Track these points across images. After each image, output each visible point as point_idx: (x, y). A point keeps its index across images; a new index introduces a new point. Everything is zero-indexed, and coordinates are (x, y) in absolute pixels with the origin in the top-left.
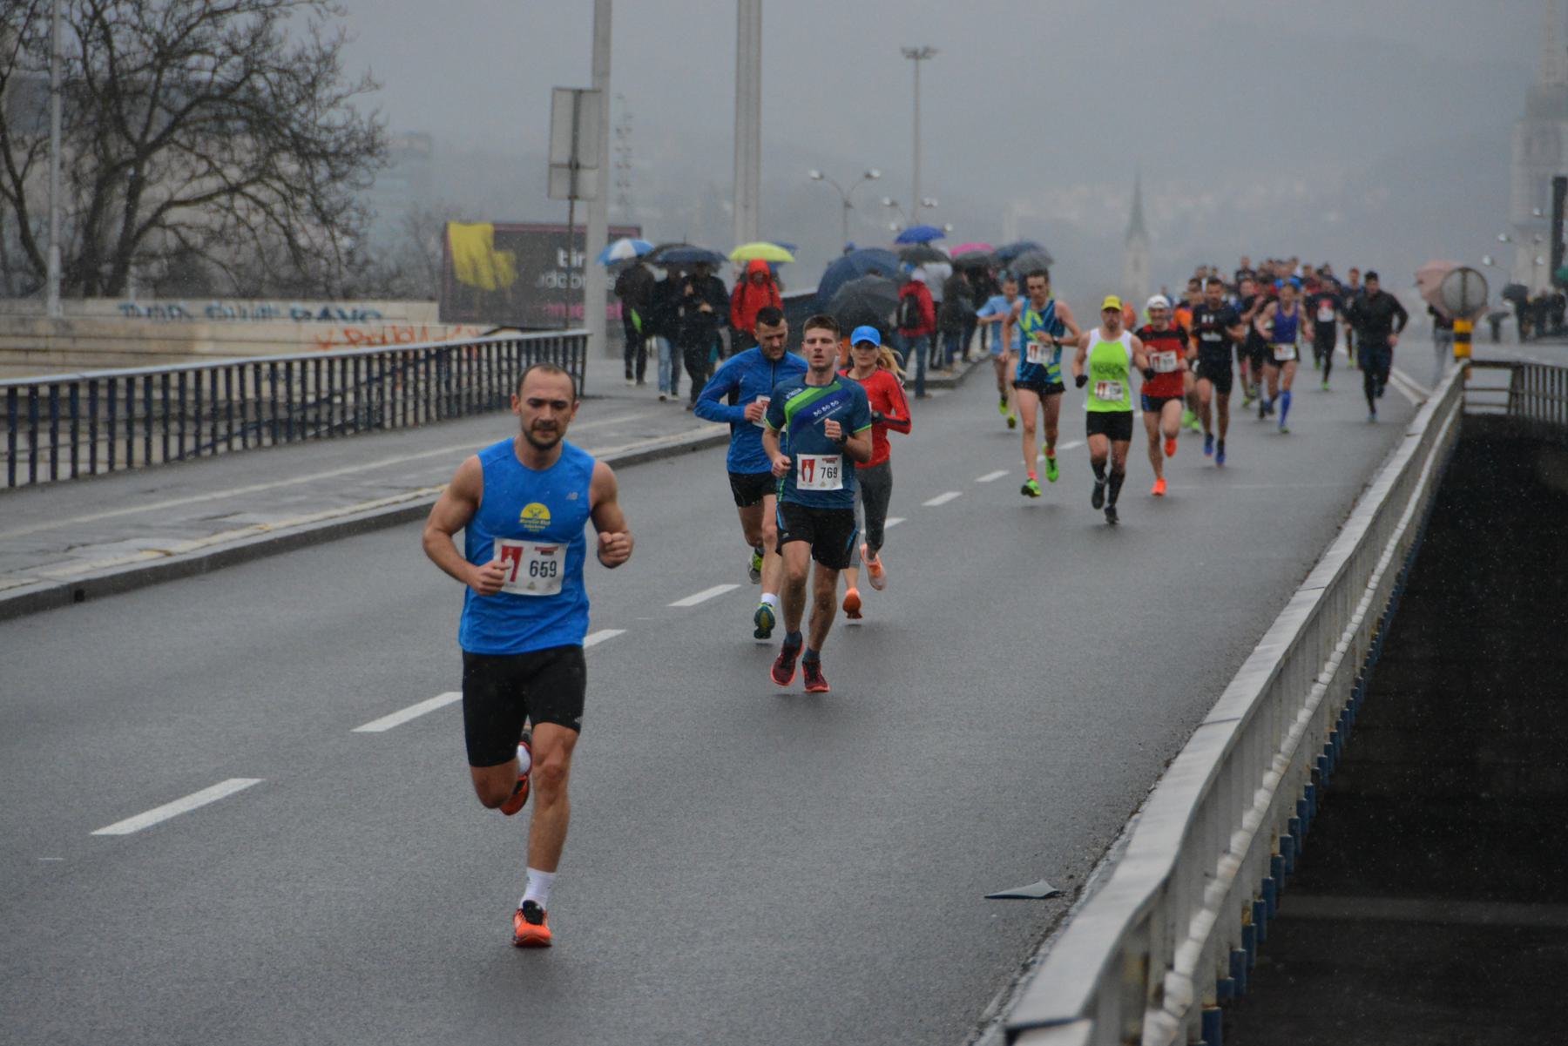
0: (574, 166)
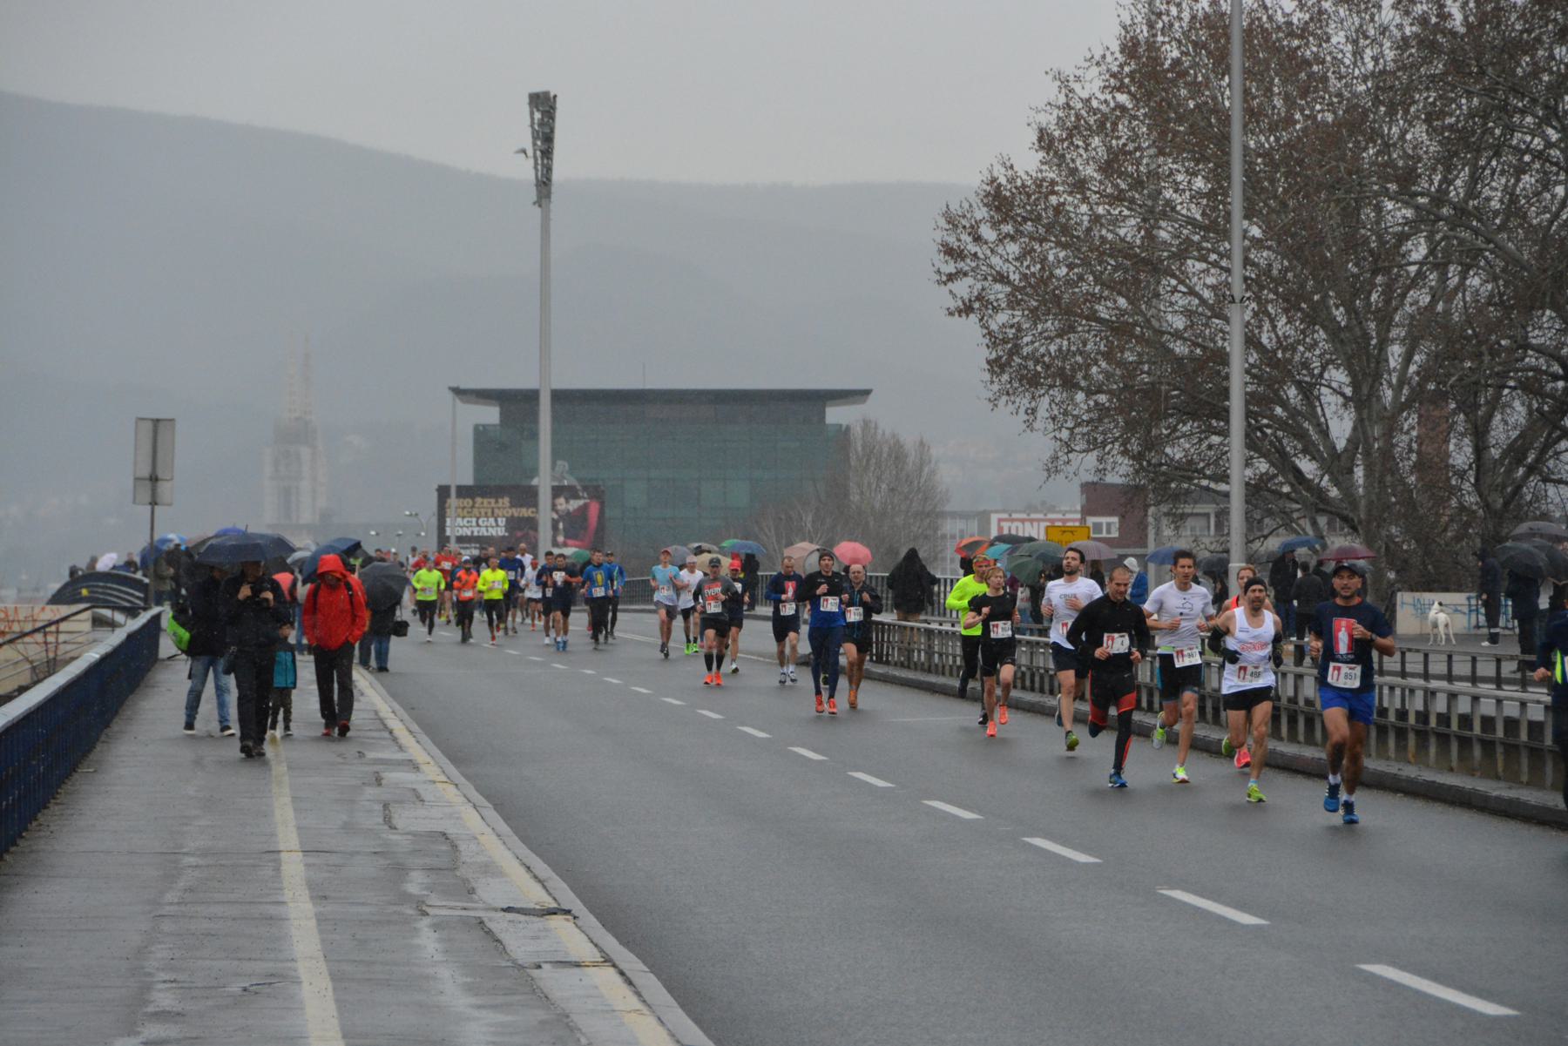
0: (154, 479)
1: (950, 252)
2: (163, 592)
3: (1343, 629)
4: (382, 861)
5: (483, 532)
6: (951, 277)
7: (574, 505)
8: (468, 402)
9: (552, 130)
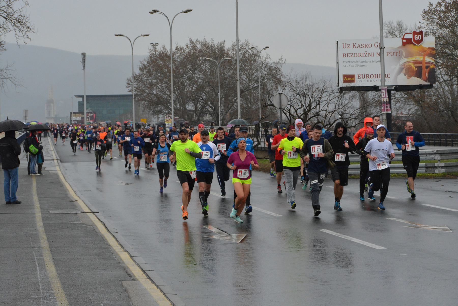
0: (26, 117)
1: (128, 84)
3: (410, 139)
5: (77, 119)
6: (128, 87)
7: (91, 115)
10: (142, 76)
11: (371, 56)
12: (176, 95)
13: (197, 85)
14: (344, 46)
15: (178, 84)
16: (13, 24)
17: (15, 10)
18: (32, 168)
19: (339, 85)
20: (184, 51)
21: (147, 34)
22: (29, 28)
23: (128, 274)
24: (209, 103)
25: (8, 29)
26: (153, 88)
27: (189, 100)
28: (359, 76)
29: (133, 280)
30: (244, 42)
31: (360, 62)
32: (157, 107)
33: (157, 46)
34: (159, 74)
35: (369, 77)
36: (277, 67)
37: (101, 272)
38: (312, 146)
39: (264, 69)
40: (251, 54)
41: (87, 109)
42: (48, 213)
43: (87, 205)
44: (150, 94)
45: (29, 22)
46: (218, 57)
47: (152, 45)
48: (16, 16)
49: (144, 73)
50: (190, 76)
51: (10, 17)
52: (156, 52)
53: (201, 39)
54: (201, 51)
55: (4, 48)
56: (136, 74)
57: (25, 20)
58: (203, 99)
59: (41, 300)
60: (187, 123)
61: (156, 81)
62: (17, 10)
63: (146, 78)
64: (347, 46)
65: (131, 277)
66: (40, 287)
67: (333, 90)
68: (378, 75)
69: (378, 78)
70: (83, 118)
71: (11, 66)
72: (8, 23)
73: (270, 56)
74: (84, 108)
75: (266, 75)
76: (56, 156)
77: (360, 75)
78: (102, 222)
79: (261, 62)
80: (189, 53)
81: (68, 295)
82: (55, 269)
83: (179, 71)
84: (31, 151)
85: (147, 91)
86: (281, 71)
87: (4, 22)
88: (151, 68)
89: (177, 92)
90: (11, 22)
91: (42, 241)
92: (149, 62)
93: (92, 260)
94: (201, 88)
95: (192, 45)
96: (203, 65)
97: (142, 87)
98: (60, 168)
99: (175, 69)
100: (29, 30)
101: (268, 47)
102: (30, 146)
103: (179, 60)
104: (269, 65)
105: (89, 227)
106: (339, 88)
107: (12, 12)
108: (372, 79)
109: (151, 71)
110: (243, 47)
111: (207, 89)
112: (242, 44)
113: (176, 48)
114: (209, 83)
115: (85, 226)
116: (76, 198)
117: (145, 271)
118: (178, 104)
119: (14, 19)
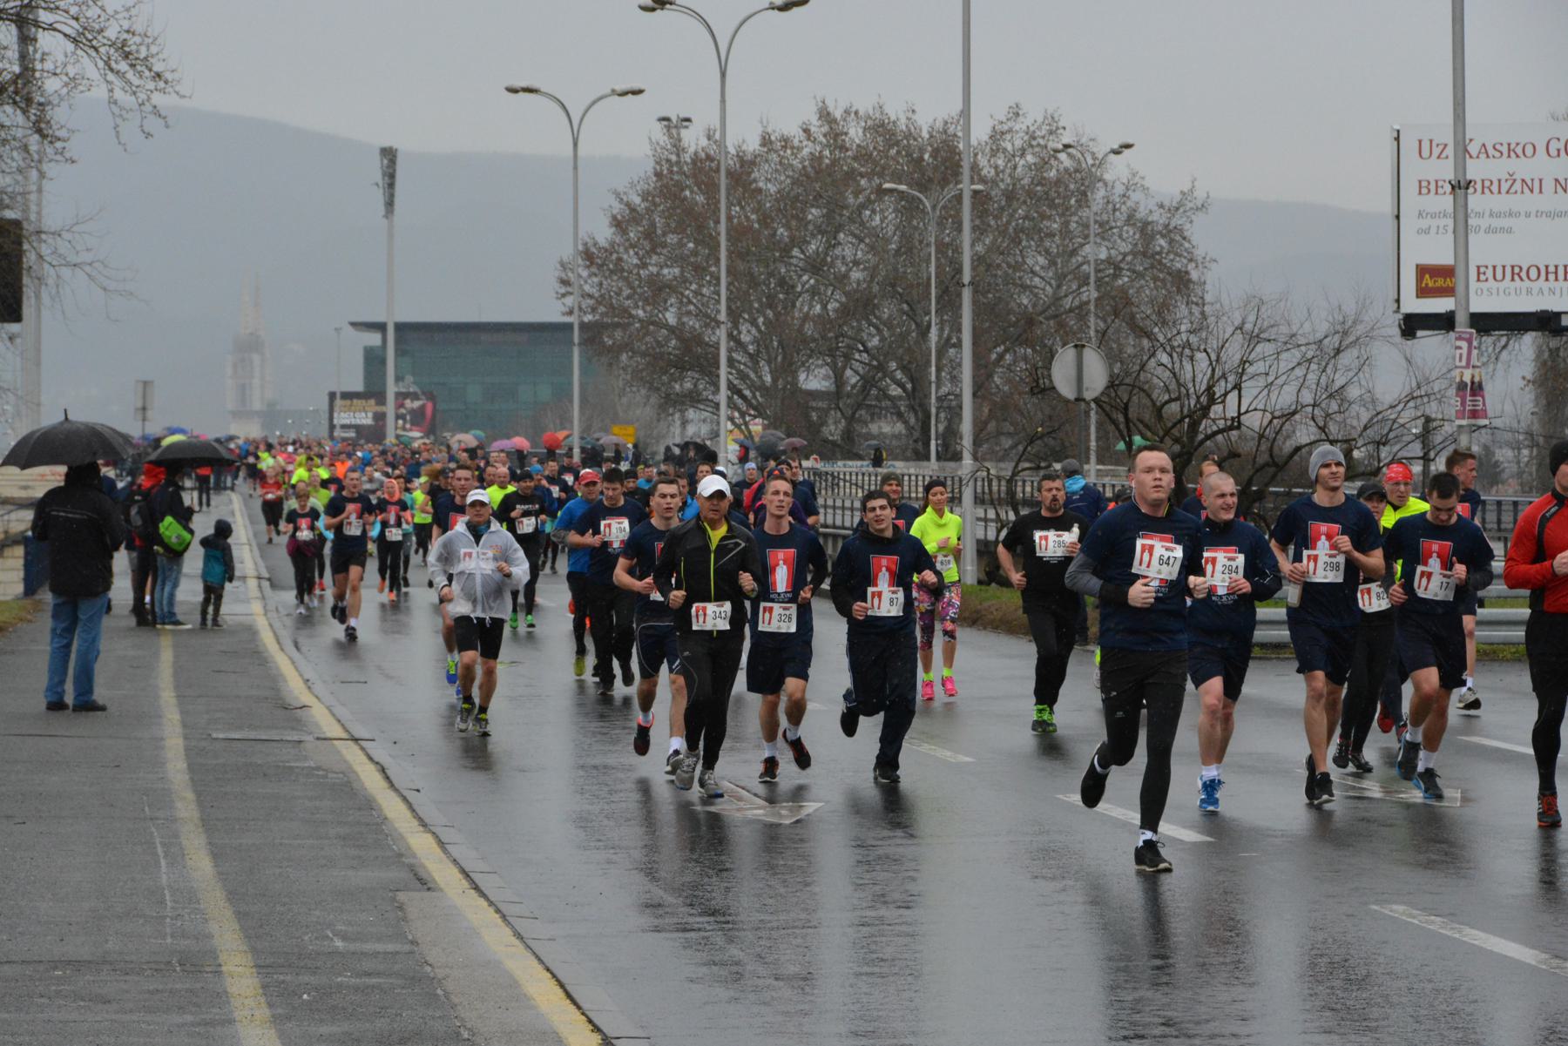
0: (144, 409)
1: (565, 282)
2: (676, 472)
4: (301, 640)
6: (564, 295)
7: (417, 404)
8: (360, 330)
9: (395, 170)
10: (622, 249)
11: (1532, 191)
12: (759, 331)
13: (846, 294)
14: (1426, 153)
15: (768, 286)
16: (101, 64)
17: (110, 11)
18: (165, 602)
19: (1399, 307)
20: (792, 154)
21: (636, 86)
22: (160, 79)
23: (420, 880)
24: (893, 365)
25: (85, 82)
26: (666, 302)
27: (812, 351)
28: (1482, 270)
29: (429, 889)
30: (1040, 120)
31: (1487, 214)
32: (682, 379)
33: (687, 127)
34: (691, 245)
35: (1523, 275)
36: (1171, 227)
37: (343, 873)
38: (1139, 543)
39: (1121, 230)
40: (1066, 170)
41: (399, 379)
42: (205, 739)
43: (339, 721)
44: (652, 323)
45: (160, 56)
46: (930, 180)
47: (665, 123)
48: (112, 33)
49: (628, 240)
50: (817, 253)
51: (90, 37)
52: (678, 155)
53: (865, 105)
54: (863, 155)
55: (68, 155)
56: (595, 244)
57: (148, 47)
58: (866, 350)
59: (168, 920)
60: (795, 449)
61: (677, 271)
62: (120, 9)
63: (635, 261)
64: (1436, 151)
65: (423, 883)
66: (167, 898)
67: (1294, 335)
68: (1556, 267)
69: (1556, 279)
70: (380, 418)
71: (91, 219)
72: (86, 60)
73: (1143, 178)
74: (385, 374)
75: (1129, 258)
76: (256, 564)
77: (1487, 267)
78: (377, 763)
79: (1108, 202)
80: (816, 159)
81: (240, 912)
82: (199, 815)
83: (774, 234)
84: (166, 540)
85: (641, 313)
86: (1189, 242)
87: (69, 55)
88: (657, 219)
89: (761, 320)
90: (94, 54)
91: (179, 805)
92: (649, 193)
93: (322, 849)
94: (861, 305)
95: (825, 129)
96: (874, 211)
97: (618, 294)
98: (265, 607)
99: (756, 226)
100: (162, 84)
101: (1128, 146)
102: (162, 520)
103: (772, 188)
104: (1138, 216)
105: (335, 775)
106: (1401, 317)
107: (99, 16)
108: (1535, 286)
109: (659, 232)
110: (1034, 138)
111: (887, 310)
112: (1032, 129)
113: (764, 138)
114: (893, 286)
115: (321, 773)
116: (306, 698)
117: (471, 874)
118: (767, 368)
119: (104, 45)
